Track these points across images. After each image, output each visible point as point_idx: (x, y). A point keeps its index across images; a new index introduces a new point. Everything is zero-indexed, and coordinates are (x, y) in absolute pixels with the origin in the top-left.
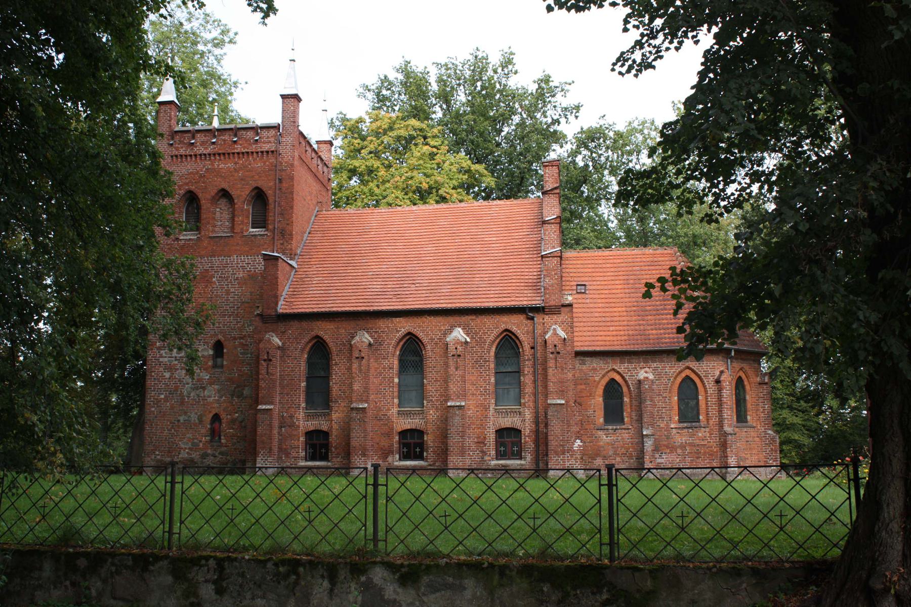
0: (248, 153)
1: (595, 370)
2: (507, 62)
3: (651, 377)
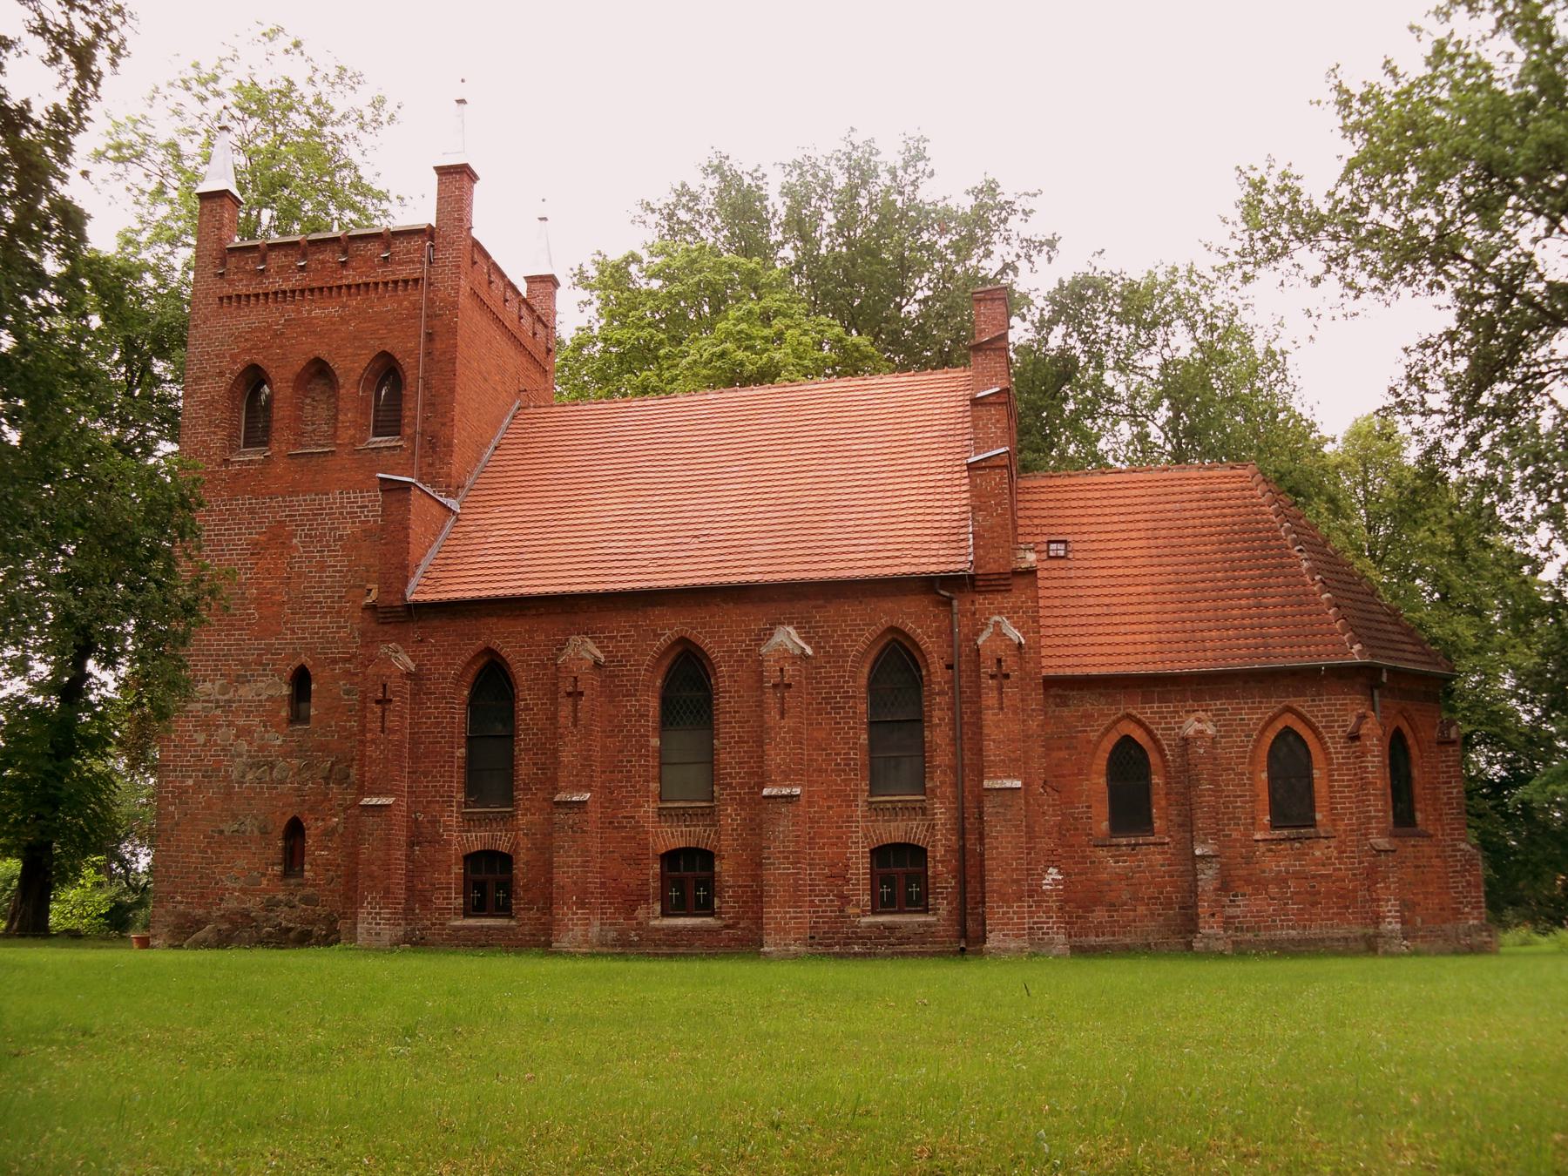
0: (367, 285)
1: (1088, 716)
2: (916, 156)
3: (1210, 730)
